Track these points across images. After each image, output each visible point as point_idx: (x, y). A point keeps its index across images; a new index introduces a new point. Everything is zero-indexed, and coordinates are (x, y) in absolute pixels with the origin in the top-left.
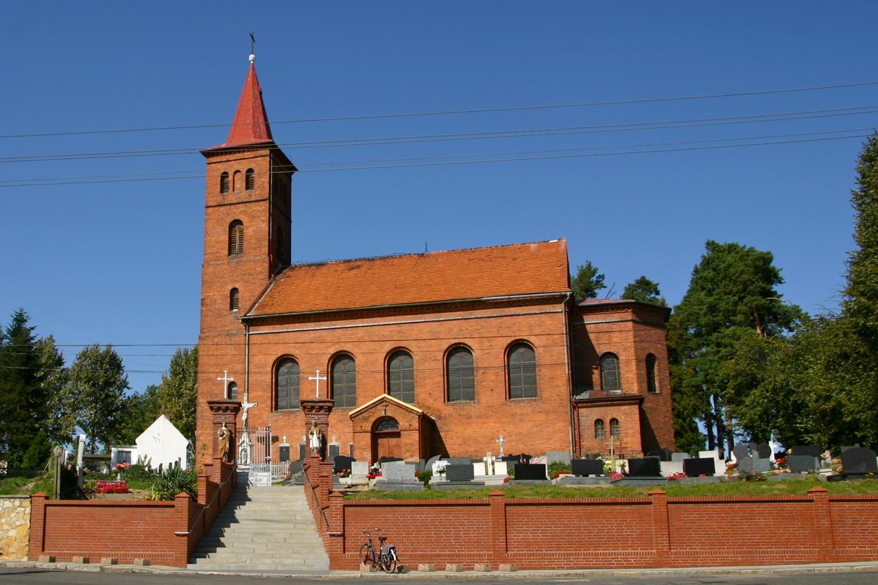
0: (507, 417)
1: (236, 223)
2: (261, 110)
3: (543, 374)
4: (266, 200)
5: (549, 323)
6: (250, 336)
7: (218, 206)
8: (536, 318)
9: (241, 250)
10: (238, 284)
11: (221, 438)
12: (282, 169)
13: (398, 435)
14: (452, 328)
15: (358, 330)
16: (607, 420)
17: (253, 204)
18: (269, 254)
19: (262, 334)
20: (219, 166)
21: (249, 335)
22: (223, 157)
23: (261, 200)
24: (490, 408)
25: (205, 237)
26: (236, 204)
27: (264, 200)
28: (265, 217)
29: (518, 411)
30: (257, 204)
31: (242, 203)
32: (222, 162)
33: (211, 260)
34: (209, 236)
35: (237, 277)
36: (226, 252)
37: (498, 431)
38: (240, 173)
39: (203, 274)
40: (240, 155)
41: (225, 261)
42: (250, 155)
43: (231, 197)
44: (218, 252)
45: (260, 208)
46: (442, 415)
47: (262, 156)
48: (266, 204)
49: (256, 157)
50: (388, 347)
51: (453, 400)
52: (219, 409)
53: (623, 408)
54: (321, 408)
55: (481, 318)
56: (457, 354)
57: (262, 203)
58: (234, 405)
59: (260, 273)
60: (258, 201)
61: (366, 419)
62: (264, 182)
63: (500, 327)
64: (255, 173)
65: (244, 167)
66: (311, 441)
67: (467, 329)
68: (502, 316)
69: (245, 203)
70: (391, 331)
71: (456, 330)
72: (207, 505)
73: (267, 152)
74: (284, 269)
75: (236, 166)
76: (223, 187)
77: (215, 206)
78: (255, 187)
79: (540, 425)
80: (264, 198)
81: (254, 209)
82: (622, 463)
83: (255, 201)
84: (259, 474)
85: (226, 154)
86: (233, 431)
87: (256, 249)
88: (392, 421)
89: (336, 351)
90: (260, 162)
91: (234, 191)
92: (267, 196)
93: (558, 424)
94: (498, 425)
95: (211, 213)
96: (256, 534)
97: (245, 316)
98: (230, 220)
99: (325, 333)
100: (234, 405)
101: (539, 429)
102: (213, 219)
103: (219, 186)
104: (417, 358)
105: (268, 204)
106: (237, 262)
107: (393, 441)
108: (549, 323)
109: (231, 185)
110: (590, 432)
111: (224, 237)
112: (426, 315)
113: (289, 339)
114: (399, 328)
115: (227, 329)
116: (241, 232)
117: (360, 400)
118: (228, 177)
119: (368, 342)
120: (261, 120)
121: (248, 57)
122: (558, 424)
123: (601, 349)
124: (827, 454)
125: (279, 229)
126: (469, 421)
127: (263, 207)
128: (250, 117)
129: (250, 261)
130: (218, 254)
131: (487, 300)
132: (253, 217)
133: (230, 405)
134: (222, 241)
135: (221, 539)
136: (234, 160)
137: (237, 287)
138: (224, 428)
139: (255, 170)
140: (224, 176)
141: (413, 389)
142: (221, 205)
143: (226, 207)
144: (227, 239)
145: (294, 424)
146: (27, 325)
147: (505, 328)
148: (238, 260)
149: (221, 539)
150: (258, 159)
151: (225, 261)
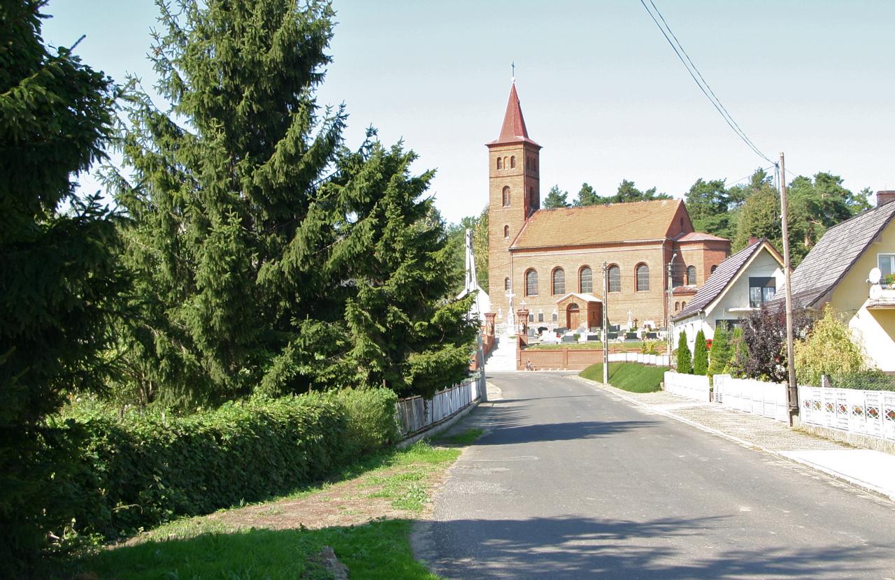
1: (506, 188)
3: (652, 280)
8: (649, 251)
12: (532, 150)
13: (578, 311)
14: (610, 256)
15: (566, 256)
16: (681, 302)
20: (496, 153)
28: (522, 185)
36: (502, 205)
50: (580, 265)
53: (688, 297)
61: (564, 304)
74: (534, 212)
82: (638, 336)
88: (575, 305)
99: (549, 257)
103: (496, 166)
107: (577, 314)
109: (503, 165)
113: (534, 260)
117: (566, 292)
119: (571, 261)
123: (688, 264)
125: (531, 188)
132: (515, 185)
141: (592, 286)
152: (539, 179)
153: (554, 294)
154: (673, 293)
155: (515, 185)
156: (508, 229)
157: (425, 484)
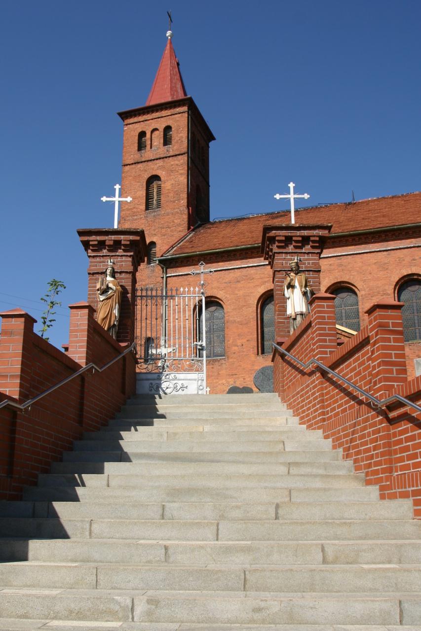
2: (178, 77)
4: (184, 154)
6: (168, 279)
7: (135, 163)
9: (159, 205)
10: (156, 237)
11: (102, 298)
12: (201, 137)
17: (171, 158)
18: (188, 207)
19: (179, 275)
20: (137, 125)
21: (167, 277)
22: (140, 117)
23: (179, 155)
26: (154, 160)
27: (185, 112)
28: (183, 170)
30: (175, 158)
31: (160, 159)
32: (140, 122)
33: (127, 217)
34: (126, 193)
35: (154, 230)
36: (143, 207)
38: (158, 132)
40: (157, 114)
41: (142, 216)
42: (167, 113)
43: (148, 154)
44: (134, 208)
47: (179, 113)
48: (185, 157)
49: (173, 115)
52: (101, 245)
54: (305, 240)
56: (409, 288)
57: (179, 157)
58: (131, 237)
59: (179, 225)
60: (176, 155)
62: (182, 137)
64: (173, 130)
65: (161, 125)
66: (289, 302)
69: (163, 158)
70: (330, 265)
71: (408, 259)
72: (20, 401)
73: (185, 108)
75: (154, 124)
76: (141, 146)
77: (132, 164)
78: (173, 142)
80: (182, 152)
81: (172, 163)
83: (173, 156)
84: (181, 376)
85: (144, 114)
86: (129, 288)
87: (174, 202)
90: (177, 119)
91: (151, 148)
92: (185, 150)
95: (129, 171)
96: (175, 493)
97: (162, 256)
98: (146, 176)
99: (252, 271)
100: (131, 237)
102: (130, 176)
103: (136, 145)
104: (363, 293)
105: (186, 158)
106: (154, 216)
109: (148, 143)
111: (141, 193)
112: (371, 246)
114: (339, 261)
115: (144, 283)
116: (159, 187)
118: (145, 136)
120: (179, 85)
121: (166, 33)
127: (182, 161)
128: (168, 82)
129: (168, 214)
132: (170, 171)
133: (122, 237)
134: (139, 197)
135: (60, 507)
136: (152, 119)
137: (154, 240)
138: (109, 278)
139: (172, 126)
140: (142, 134)
142: (138, 163)
143: (143, 163)
144: (145, 194)
145: (219, 374)
148: (155, 214)
149: (60, 507)
150: (176, 116)
151: (142, 216)
152: (120, 461)
153: (263, 353)
154: (164, 505)
155: (170, 171)
156: (173, 133)
157: (375, 208)
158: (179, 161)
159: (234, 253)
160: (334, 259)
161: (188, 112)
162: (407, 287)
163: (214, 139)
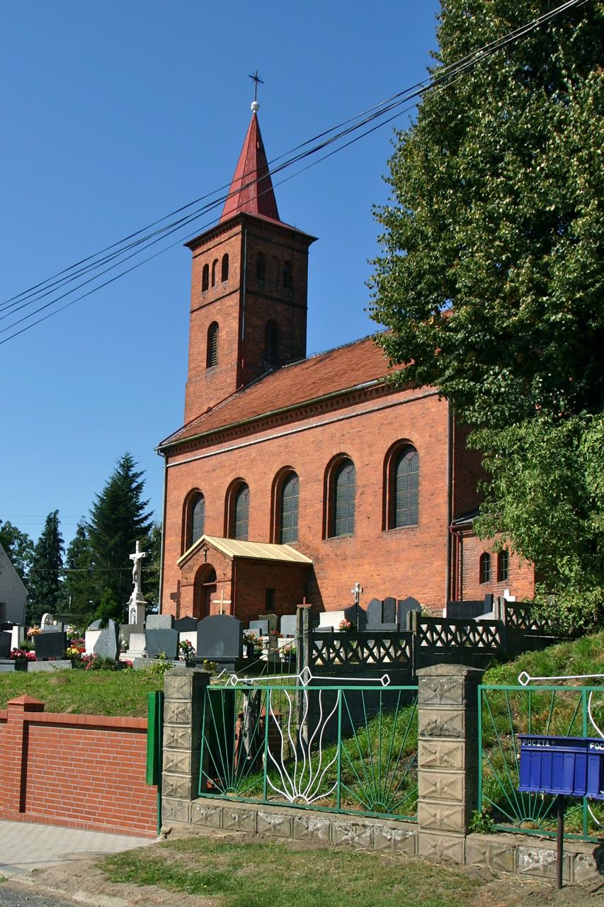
0: (382, 555)
5: (434, 410)
7: (200, 308)
17: (227, 298)
24: (366, 543)
25: (190, 349)
29: (394, 545)
31: (218, 299)
36: (204, 364)
37: (372, 576)
39: (187, 395)
45: (231, 303)
46: (320, 557)
47: (235, 235)
51: (400, 526)
55: (362, 414)
63: (382, 424)
67: (349, 432)
68: (384, 408)
79: (415, 565)
81: (228, 304)
89: (233, 479)
90: (233, 243)
93: (436, 564)
94: (372, 568)
101: (414, 571)
102: (196, 326)
108: (434, 410)
110: (473, 574)
112: (311, 419)
114: (286, 441)
122: (436, 564)
124: (264, 658)
126: (344, 563)
130: (199, 369)
131: (363, 389)
146: (133, 471)
147: (386, 425)
148: (213, 372)
158: (233, 301)
159: (359, 393)
160: (282, 438)
161: (243, 235)
162: (343, 469)
163: (310, 240)
